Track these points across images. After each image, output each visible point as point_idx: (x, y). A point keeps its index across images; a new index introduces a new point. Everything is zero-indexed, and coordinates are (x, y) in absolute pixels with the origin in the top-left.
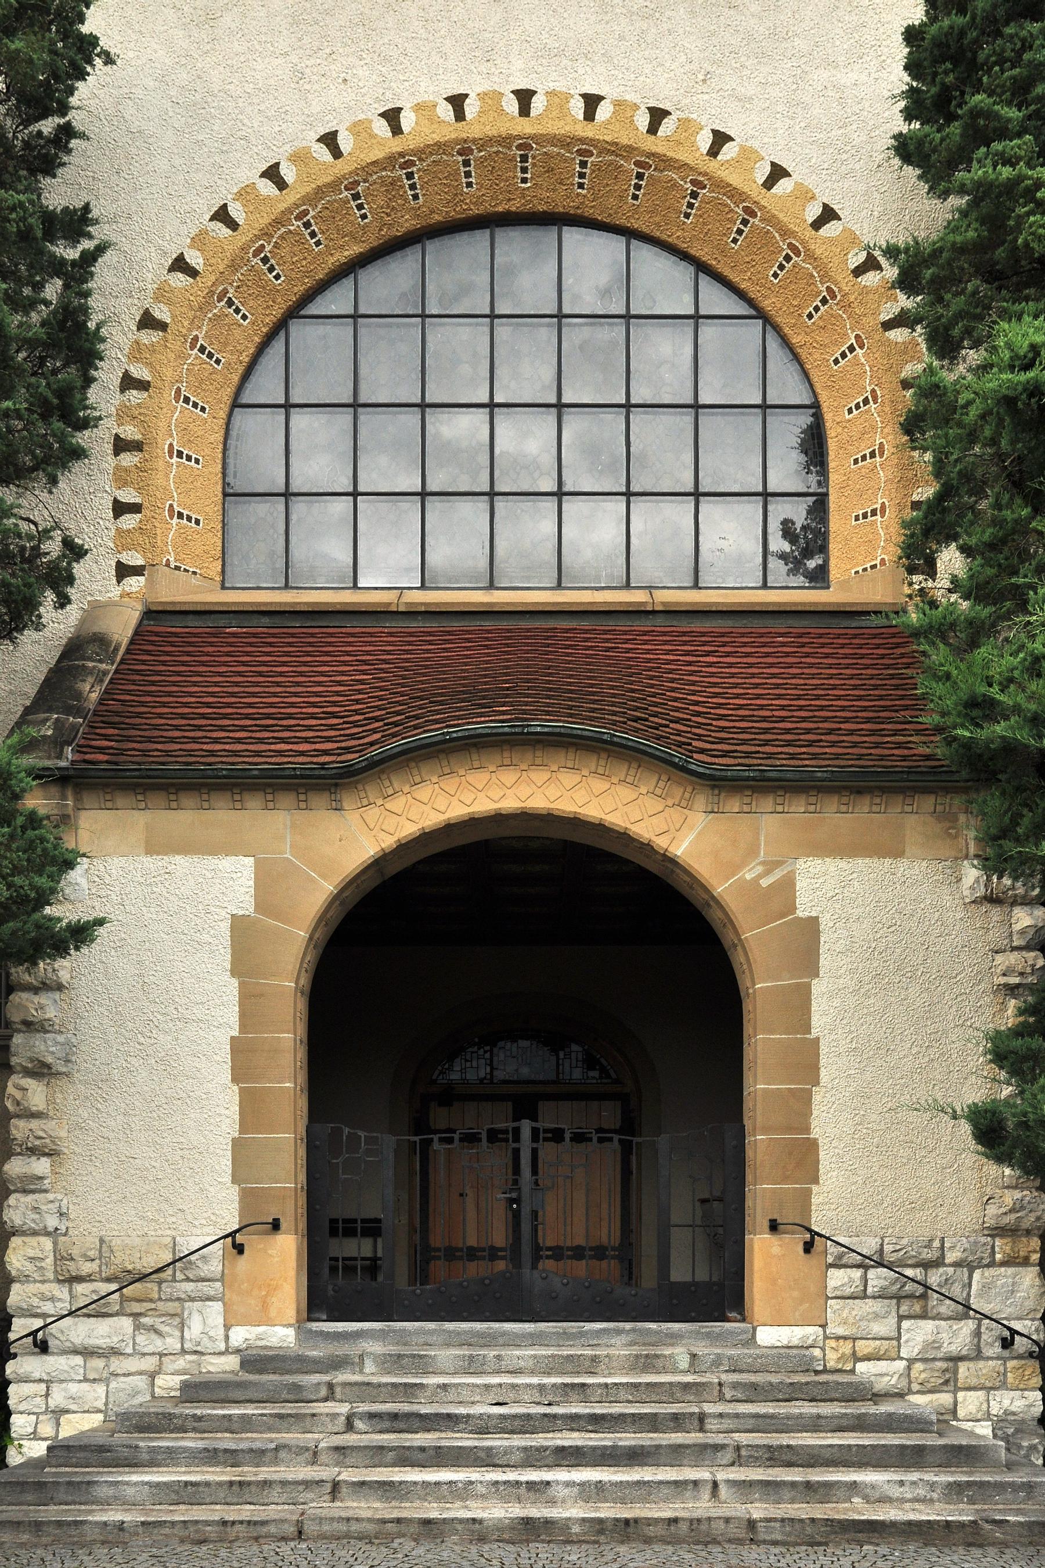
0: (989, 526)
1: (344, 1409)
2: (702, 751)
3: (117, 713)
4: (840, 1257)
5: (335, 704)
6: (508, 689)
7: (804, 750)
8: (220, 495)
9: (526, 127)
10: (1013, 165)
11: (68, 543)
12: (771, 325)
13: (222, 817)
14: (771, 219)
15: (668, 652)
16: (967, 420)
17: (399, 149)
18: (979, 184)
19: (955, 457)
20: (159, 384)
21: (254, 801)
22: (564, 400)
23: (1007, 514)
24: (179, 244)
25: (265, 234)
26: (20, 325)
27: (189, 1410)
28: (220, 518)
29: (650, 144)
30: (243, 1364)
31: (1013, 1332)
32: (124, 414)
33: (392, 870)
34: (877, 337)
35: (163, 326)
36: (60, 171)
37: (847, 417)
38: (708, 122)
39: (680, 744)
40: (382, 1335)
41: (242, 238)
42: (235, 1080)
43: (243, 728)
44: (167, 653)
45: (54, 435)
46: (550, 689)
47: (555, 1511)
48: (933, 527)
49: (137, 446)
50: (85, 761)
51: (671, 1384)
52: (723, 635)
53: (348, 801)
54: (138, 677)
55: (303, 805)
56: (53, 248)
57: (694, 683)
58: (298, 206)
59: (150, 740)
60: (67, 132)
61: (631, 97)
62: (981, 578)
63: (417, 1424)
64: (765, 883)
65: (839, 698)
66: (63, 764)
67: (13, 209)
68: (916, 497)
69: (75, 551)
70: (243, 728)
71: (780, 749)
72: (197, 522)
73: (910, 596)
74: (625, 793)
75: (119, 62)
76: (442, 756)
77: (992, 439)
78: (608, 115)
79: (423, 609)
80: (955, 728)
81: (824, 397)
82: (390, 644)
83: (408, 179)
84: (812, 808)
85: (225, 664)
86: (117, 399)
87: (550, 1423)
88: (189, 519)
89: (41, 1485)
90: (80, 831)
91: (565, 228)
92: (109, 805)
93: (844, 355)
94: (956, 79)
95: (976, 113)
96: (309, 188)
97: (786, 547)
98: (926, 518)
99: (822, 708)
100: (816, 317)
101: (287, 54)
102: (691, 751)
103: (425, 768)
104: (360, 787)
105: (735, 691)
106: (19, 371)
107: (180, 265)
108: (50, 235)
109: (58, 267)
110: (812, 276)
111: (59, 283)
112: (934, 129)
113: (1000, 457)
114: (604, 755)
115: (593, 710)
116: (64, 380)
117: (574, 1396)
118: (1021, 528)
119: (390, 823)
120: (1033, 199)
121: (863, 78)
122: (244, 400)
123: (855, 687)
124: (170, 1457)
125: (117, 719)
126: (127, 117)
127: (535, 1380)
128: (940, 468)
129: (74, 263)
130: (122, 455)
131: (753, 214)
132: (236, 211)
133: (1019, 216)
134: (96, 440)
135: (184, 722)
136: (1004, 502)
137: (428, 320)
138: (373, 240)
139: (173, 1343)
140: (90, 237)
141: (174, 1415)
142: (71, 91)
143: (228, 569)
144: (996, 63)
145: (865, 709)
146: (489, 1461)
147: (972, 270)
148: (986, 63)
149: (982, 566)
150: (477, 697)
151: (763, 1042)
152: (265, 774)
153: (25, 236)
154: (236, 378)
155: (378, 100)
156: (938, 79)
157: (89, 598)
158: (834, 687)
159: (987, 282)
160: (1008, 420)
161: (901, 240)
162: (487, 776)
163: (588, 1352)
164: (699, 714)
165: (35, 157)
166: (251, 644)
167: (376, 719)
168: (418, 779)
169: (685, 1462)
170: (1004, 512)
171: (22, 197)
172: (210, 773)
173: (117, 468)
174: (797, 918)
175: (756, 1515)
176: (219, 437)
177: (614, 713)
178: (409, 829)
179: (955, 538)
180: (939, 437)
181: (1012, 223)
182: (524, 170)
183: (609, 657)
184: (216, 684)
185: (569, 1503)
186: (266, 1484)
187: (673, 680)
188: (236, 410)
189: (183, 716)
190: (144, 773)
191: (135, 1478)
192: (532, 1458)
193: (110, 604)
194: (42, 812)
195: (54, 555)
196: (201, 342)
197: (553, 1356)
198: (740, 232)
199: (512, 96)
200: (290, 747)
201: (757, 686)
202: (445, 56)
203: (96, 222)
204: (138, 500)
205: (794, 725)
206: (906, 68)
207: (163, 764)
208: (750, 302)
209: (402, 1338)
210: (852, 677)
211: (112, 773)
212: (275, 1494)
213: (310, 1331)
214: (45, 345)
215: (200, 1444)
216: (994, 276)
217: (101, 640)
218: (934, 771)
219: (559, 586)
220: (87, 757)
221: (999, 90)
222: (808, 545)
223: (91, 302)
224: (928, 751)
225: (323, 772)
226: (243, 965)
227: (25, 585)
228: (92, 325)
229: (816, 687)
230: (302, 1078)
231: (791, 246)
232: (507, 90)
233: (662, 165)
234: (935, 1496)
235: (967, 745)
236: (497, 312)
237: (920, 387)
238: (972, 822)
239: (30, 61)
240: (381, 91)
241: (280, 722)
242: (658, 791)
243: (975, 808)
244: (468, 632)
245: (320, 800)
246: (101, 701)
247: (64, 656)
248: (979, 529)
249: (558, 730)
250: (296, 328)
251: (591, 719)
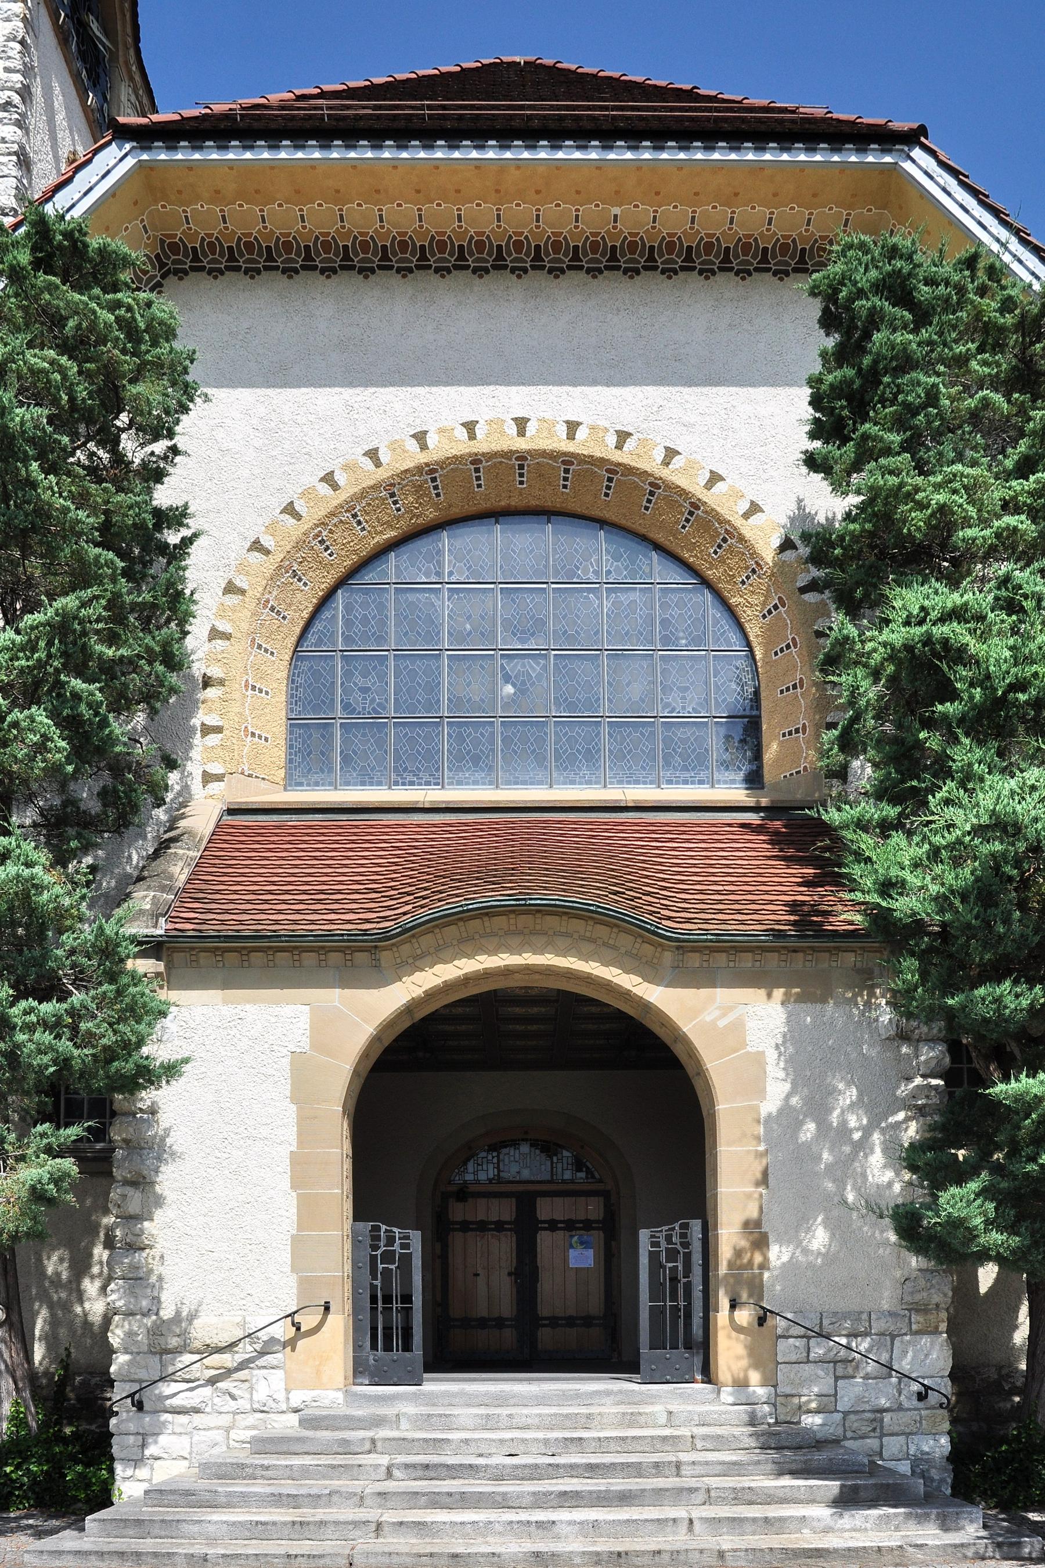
1: (384, 1460)
2: (669, 918)
4: (788, 1330)
5: (374, 881)
27: (259, 1460)
30: (301, 1422)
31: (927, 1388)
33: (420, 1015)
35: (243, 592)
36: (166, 480)
39: (651, 913)
40: (414, 1398)
42: (293, 1187)
44: (242, 842)
47: (560, 1545)
51: (652, 1437)
61: (603, 423)
63: (444, 1472)
64: (721, 1024)
72: (266, 740)
87: (554, 1470)
88: (260, 737)
89: (139, 1522)
95: (865, 437)
96: (356, 489)
117: (573, 1448)
120: (913, 500)
124: (244, 1500)
127: (540, 1435)
138: (404, 525)
139: (243, 1404)
140: (188, 527)
141: (247, 1466)
146: (504, 1504)
154: (298, 630)
163: (584, 1410)
166: (308, 834)
167: (408, 894)
169: (666, 1502)
174: (748, 1053)
175: (725, 1547)
177: (599, 888)
183: (593, 844)
185: (570, 1540)
186: (322, 1523)
189: (253, 892)
191: (215, 1517)
192: (540, 1501)
197: (555, 1415)
204: (220, 724)
209: (431, 1399)
212: (329, 1531)
213: (355, 1394)
215: (268, 1490)
223: (187, 574)
226: (302, 1092)
228: (188, 592)
230: (348, 1185)
234: (868, 1526)
246: (189, 881)
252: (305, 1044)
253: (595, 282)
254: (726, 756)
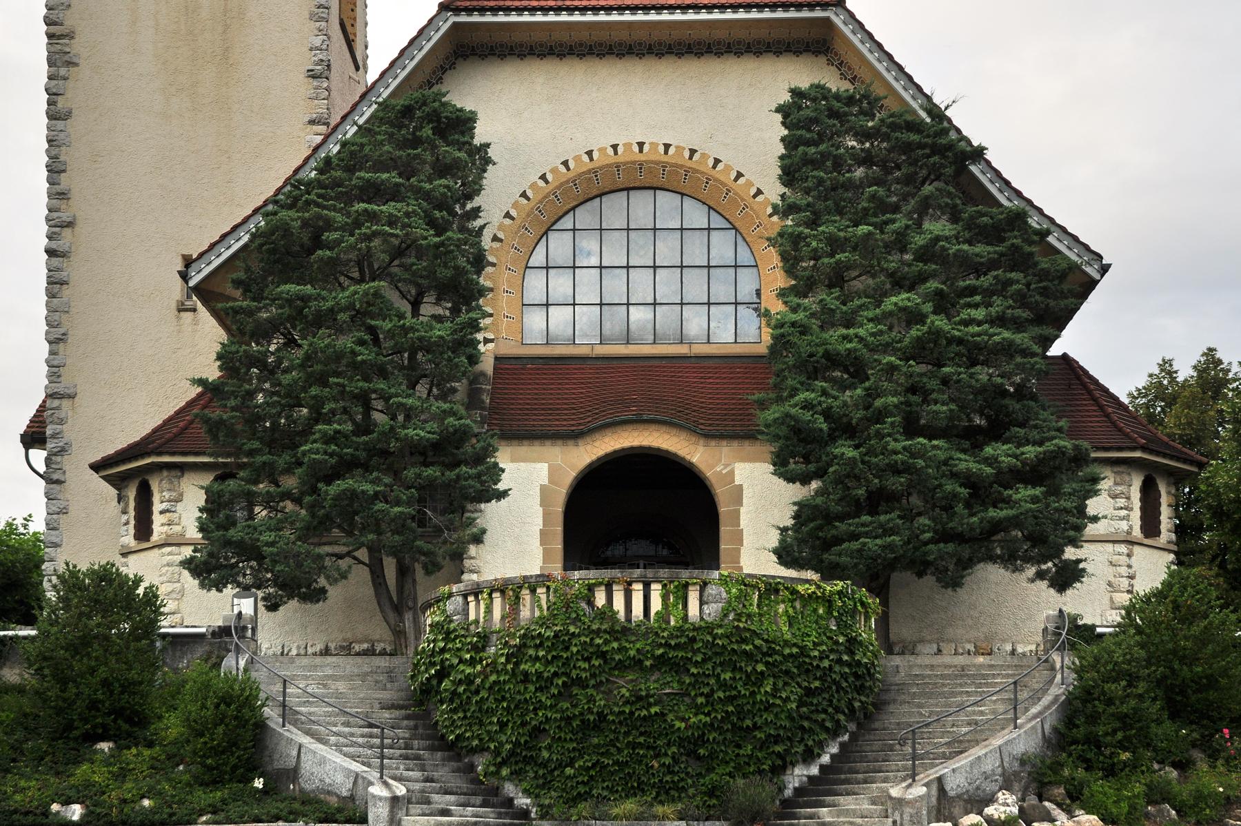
9: (642, 157)
13: (536, 449)
25: (540, 202)
29: (689, 164)
35: (501, 241)
41: (532, 204)
53: (580, 442)
74: (675, 439)
96: (557, 184)
107: (508, 215)
119: (595, 450)
151: (724, 530)
178: (601, 453)
226: (544, 503)
232: (634, 142)
245: (571, 442)
250: (550, 233)
252: (546, 482)
253: (680, 61)
254: (234, 664)
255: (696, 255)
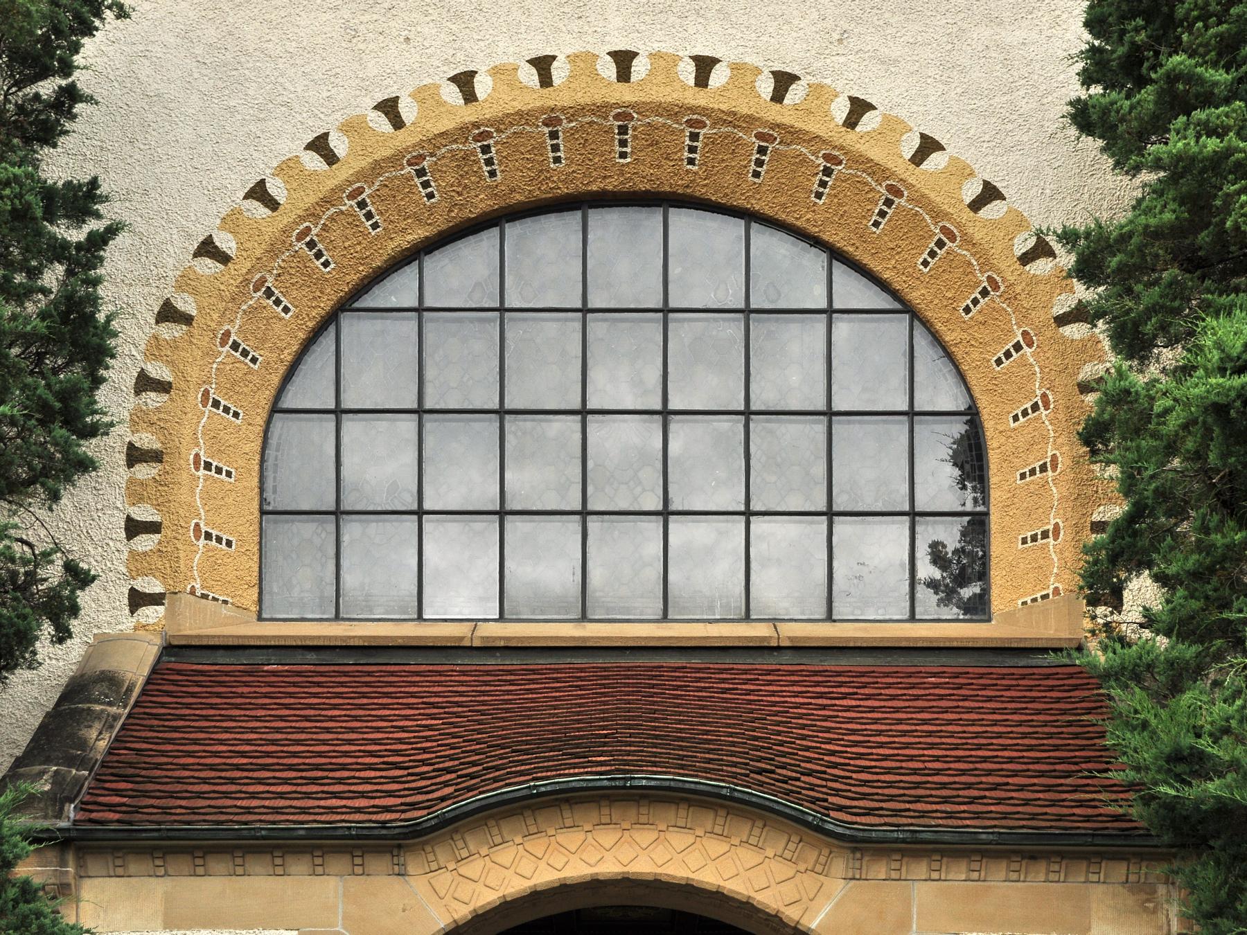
0: (1192, 552)
2: (840, 808)
3: (131, 765)
5: (397, 753)
6: (606, 736)
7: (963, 808)
8: (257, 513)
9: (625, 94)
10: (1221, 136)
11: (71, 568)
12: (920, 320)
14: (920, 200)
15: (797, 694)
16: (1164, 430)
17: (473, 119)
18: (1179, 158)
19: (1150, 472)
20: (183, 385)
21: (299, 866)
22: (671, 406)
23: (1217, 538)
24: (208, 225)
25: (312, 215)
26: (14, 317)
28: (257, 539)
29: (774, 113)
32: (139, 419)
34: (1049, 334)
35: (187, 319)
36: (61, 140)
37: (1012, 425)
38: (846, 88)
39: (814, 801)
41: (283, 218)
43: (286, 781)
44: (193, 695)
45: (56, 444)
46: (656, 737)
48: (1122, 553)
49: (155, 457)
50: (91, 821)
52: (863, 674)
53: (414, 865)
54: (156, 722)
55: (358, 870)
56: (54, 229)
57: (828, 730)
58: (351, 183)
59: (171, 795)
60: (71, 95)
61: (752, 60)
62: (1184, 612)
65: (1005, 748)
66: (63, 824)
67: (7, 184)
68: (1096, 517)
69: (79, 577)
70: (286, 781)
71: (935, 807)
72: (229, 544)
73: (1093, 632)
74: (748, 856)
75: (133, 14)
76: (528, 813)
77: (1197, 452)
78: (724, 80)
79: (502, 644)
80: (1156, 784)
81: (983, 403)
82: (462, 683)
83: (484, 152)
84: (975, 875)
85: (263, 707)
86: (132, 401)
88: (219, 540)
90: (81, 904)
91: (671, 210)
92: (120, 871)
93: (1008, 355)
94: (1149, 37)
95: (1173, 78)
96: (364, 163)
97: (937, 574)
98: (1113, 542)
99: (985, 759)
100: (974, 310)
101: (336, 8)
102: (827, 808)
103: (506, 826)
104: (428, 849)
105: (878, 739)
106: (17, 372)
107: (207, 249)
108: (50, 216)
109: (59, 251)
110: (970, 264)
111: (60, 269)
112: (1123, 95)
113: (1207, 472)
114: (722, 812)
115: (709, 761)
116: (69, 381)
118: (1233, 554)
119: (465, 890)
121: (1034, 35)
122: (289, 402)
123: (1025, 736)
125: (131, 771)
126: (143, 78)
128: (1131, 485)
129: (79, 246)
130: (137, 467)
131: (899, 194)
132: (276, 188)
133: (1228, 195)
134: (106, 450)
135: (213, 774)
136: (1211, 525)
137: (507, 315)
138: (441, 223)
140: (98, 216)
142: (76, 48)
143: (266, 597)
144: (1197, 19)
145: (1037, 761)
147: (1169, 257)
148: (1186, 18)
149: (1185, 598)
150: (574, 747)
152: (312, 834)
153: (21, 215)
154: (276, 380)
155: (446, 62)
156: (1127, 38)
157: (95, 631)
158: (1000, 735)
159: (1187, 271)
160: (1217, 431)
161: (1080, 223)
162: (581, 836)
164: (835, 766)
165: (31, 124)
166: (294, 684)
167: (448, 771)
168: (498, 839)
170: (1213, 536)
171: (16, 170)
172: (245, 833)
173: (131, 481)
176: (256, 445)
177: (735, 765)
178: (487, 897)
179: (1149, 565)
180: (1127, 449)
181: (1218, 203)
182: (623, 143)
183: (726, 700)
184: (253, 730)
187: (803, 727)
188: (277, 415)
189: (212, 767)
190: (164, 834)
193: (121, 638)
194: (37, 881)
195: (55, 581)
196: (233, 337)
198: (882, 214)
199: (609, 58)
200: (343, 802)
201: (904, 733)
202: (527, 12)
203: (105, 199)
204: (157, 518)
205: (952, 779)
206: (1087, 24)
207: (189, 823)
208: (895, 294)
210: (1020, 724)
211: (125, 835)
214: (45, 340)
216: (1194, 263)
217: (111, 680)
218: (1126, 834)
219: (665, 618)
220: (94, 815)
221: (1201, 50)
222: (965, 573)
223: (101, 291)
224: (1121, 811)
225: (384, 832)
227: (18, 617)
228: (101, 317)
229: (978, 735)
231: (944, 230)
232: (602, 51)
233: (789, 138)
235: (1170, 805)
236: (590, 306)
237: (1106, 393)
238: (1175, 895)
239: (28, 14)
240: (451, 52)
241: (331, 774)
242: (788, 854)
243: (1179, 880)
244: (557, 671)
245: (379, 864)
246: (111, 751)
247: (64, 698)
248: (1180, 556)
249: (667, 784)
250: (350, 325)
251: (706, 770)
255: (791, 372)
